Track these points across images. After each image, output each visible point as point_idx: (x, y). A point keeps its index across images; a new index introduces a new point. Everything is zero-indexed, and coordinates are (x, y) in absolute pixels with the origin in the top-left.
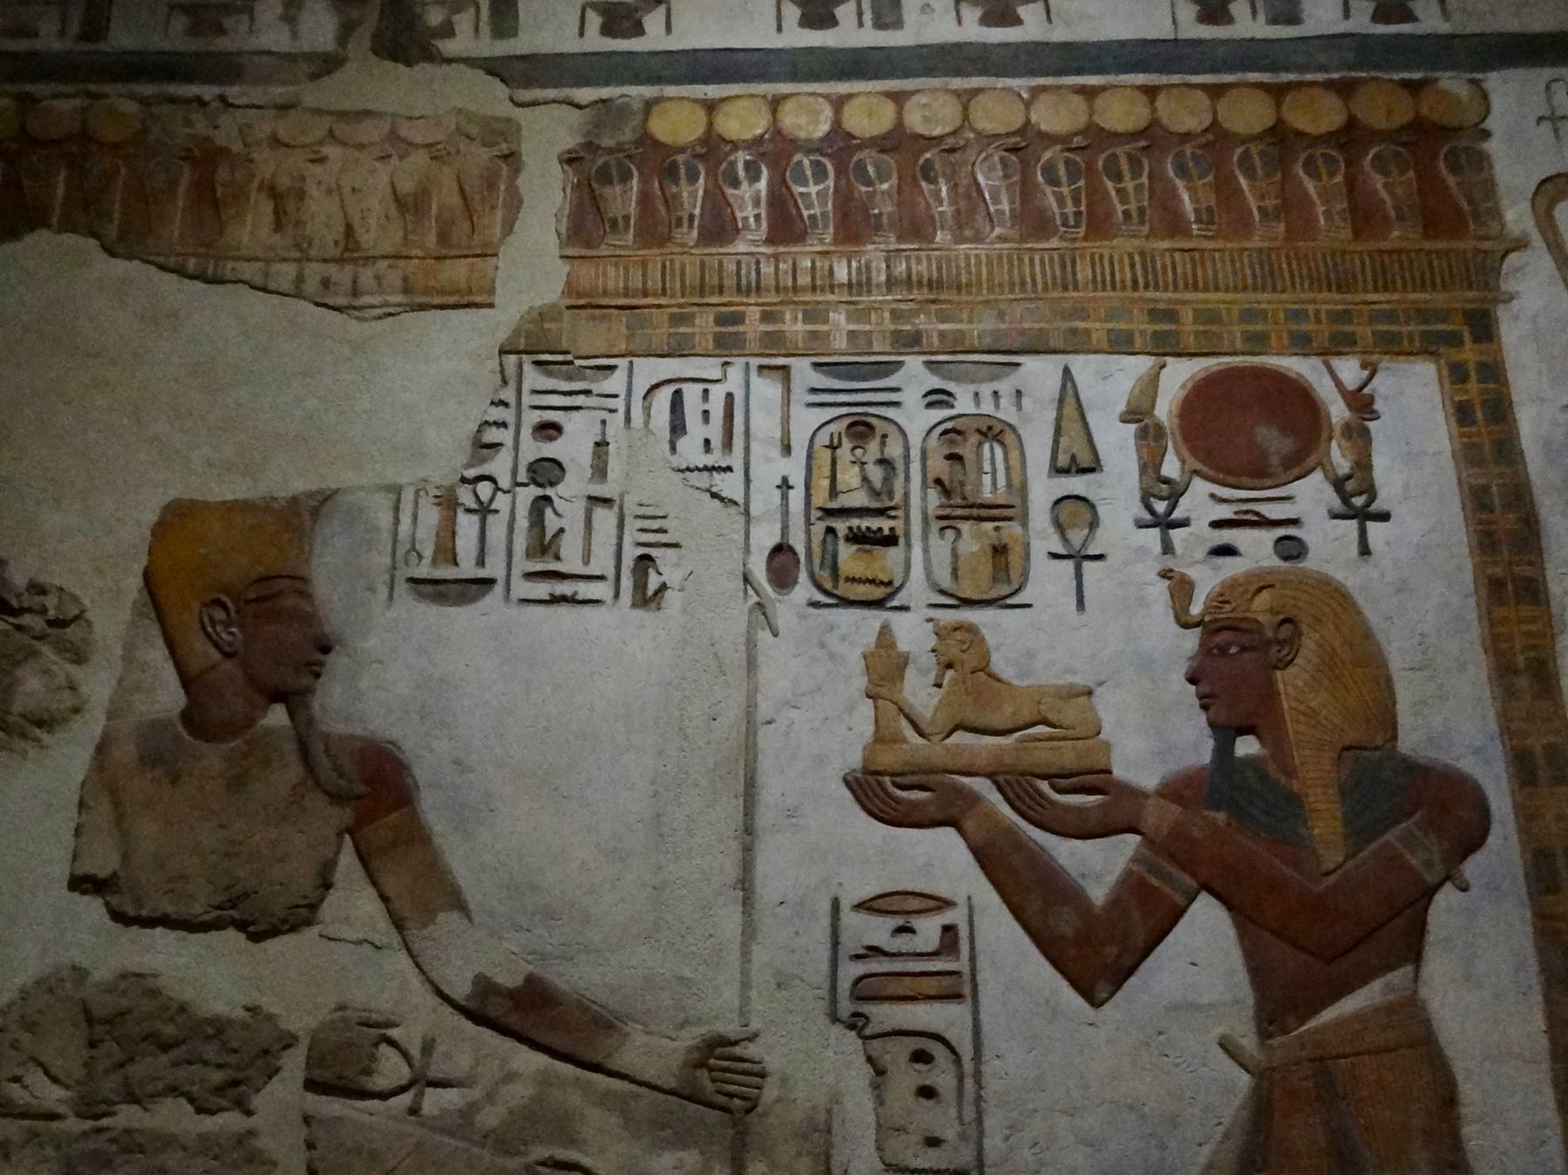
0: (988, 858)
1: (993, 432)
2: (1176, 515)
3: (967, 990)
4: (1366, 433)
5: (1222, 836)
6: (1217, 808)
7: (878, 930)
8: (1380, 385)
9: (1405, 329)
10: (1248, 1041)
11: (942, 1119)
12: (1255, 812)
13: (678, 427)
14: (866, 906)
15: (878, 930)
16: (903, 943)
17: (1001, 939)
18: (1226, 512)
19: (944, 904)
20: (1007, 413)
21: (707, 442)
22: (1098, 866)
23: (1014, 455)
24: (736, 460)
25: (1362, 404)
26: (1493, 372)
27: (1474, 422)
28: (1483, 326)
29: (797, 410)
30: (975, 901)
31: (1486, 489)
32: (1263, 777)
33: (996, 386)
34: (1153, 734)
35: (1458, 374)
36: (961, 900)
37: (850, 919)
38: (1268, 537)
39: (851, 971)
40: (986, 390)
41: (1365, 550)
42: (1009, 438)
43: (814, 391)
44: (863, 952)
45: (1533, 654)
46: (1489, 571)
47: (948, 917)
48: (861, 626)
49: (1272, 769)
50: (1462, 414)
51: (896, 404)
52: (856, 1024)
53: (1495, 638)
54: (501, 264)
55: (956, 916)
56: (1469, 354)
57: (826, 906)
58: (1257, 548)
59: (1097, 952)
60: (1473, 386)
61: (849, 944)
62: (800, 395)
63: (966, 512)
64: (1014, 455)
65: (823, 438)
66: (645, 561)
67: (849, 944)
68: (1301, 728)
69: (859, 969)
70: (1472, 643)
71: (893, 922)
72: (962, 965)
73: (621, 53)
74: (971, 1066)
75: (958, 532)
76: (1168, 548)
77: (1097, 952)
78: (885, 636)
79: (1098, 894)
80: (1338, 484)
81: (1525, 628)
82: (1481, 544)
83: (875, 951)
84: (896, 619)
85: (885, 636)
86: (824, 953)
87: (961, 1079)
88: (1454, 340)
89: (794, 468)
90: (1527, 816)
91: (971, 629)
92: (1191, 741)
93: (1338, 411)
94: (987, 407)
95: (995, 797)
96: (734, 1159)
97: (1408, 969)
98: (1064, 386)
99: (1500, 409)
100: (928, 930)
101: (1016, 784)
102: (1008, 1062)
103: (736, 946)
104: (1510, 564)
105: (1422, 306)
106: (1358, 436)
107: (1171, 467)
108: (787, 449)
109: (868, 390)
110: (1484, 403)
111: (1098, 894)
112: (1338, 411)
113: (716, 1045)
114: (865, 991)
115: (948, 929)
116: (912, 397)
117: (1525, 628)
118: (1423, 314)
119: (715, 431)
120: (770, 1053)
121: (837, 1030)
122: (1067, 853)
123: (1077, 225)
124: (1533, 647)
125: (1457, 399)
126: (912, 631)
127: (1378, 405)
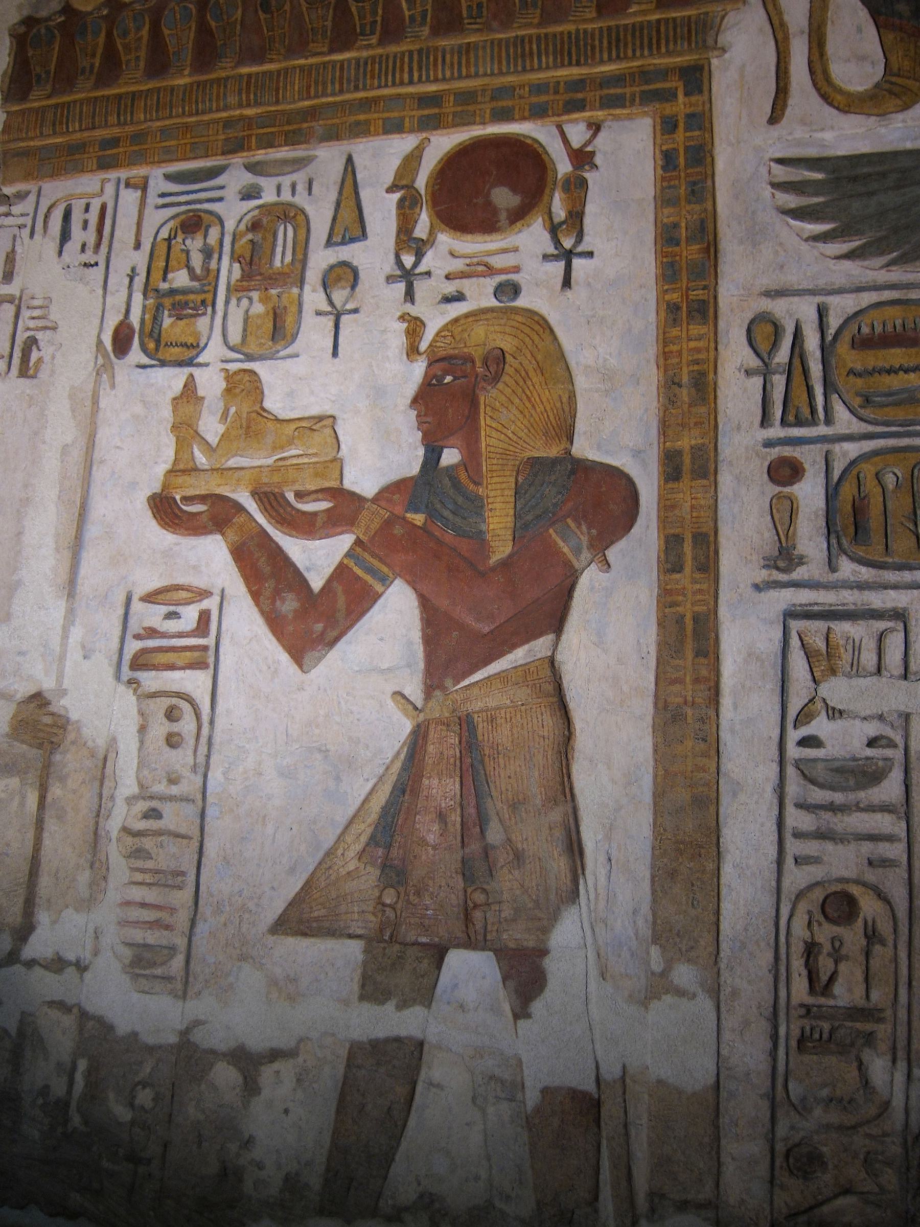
0: (241, 555)
1: (288, 213)
2: (421, 269)
3: (211, 660)
4: (583, 184)
5: (419, 531)
6: (416, 511)
7: (153, 616)
8: (602, 142)
9: (628, 90)
10: (414, 690)
11: (181, 759)
12: (446, 513)
13: (65, 236)
14: (150, 598)
15: (153, 616)
16: (172, 626)
17: (244, 627)
18: (458, 265)
19: (205, 594)
20: (301, 199)
21: (84, 246)
22: (317, 558)
23: (302, 232)
24: (101, 258)
25: (582, 158)
26: (701, 121)
27: (675, 168)
28: (696, 78)
29: (149, 210)
30: (226, 592)
31: (676, 226)
32: (456, 484)
33: (294, 177)
34: (379, 453)
35: (668, 126)
36: (216, 591)
37: (137, 606)
38: (490, 283)
39: (133, 646)
40: (286, 181)
41: (567, 282)
42: (300, 218)
43: (163, 195)
44: (142, 632)
45: (696, 368)
46: (667, 297)
47: (205, 604)
48: (171, 380)
49: (463, 476)
50: (668, 160)
51: (221, 199)
52: (132, 683)
53: (666, 355)
54: (886, 709)
55: (211, 604)
56: (681, 106)
57: (122, 598)
58: (481, 294)
59: (310, 620)
60: (680, 135)
61: (134, 626)
62: (152, 199)
63: (586, 926)
64: (302, 232)
65: (164, 234)
66: (32, 342)
67: (134, 626)
68: (492, 442)
69: (138, 645)
70: (648, 361)
71: (164, 609)
72: (210, 641)
73: (188, 159)
74: (206, 724)
75: (250, 299)
76: (410, 296)
77: (310, 620)
78: (190, 386)
79: (317, 583)
80: (554, 230)
81: (692, 344)
82: (663, 275)
83: (152, 633)
84: (196, 372)
85: (190, 386)
86: (117, 632)
87: (199, 728)
88: (669, 96)
89: (141, 259)
90: (666, 507)
91: (252, 372)
92: (408, 459)
93: (564, 167)
94: (286, 196)
95: (252, 506)
96: (41, 785)
97: (550, 638)
98: (346, 169)
99: (701, 156)
100: (190, 615)
101: (270, 500)
102: (234, 708)
103: (59, 630)
104: (688, 289)
105: (646, 69)
106: (577, 188)
107: (421, 230)
108: (138, 246)
109: (200, 191)
110: (687, 149)
111: (317, 583)
112: (564, 167)
113: (38, 699)
114: (140, 662)
115: (204, 617)
116: (231, 192)
117: (692, 344)
118: (645, 75)
119: (91, 237)
120: (73, 706)
121: (122, 688)
122: (296, 549)
123: (373, 33)
124: (697, 362)
125: (664, 148)
126: (210, 382)
127: (598, 160)
